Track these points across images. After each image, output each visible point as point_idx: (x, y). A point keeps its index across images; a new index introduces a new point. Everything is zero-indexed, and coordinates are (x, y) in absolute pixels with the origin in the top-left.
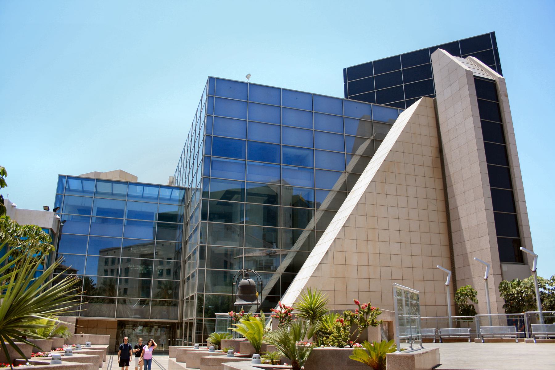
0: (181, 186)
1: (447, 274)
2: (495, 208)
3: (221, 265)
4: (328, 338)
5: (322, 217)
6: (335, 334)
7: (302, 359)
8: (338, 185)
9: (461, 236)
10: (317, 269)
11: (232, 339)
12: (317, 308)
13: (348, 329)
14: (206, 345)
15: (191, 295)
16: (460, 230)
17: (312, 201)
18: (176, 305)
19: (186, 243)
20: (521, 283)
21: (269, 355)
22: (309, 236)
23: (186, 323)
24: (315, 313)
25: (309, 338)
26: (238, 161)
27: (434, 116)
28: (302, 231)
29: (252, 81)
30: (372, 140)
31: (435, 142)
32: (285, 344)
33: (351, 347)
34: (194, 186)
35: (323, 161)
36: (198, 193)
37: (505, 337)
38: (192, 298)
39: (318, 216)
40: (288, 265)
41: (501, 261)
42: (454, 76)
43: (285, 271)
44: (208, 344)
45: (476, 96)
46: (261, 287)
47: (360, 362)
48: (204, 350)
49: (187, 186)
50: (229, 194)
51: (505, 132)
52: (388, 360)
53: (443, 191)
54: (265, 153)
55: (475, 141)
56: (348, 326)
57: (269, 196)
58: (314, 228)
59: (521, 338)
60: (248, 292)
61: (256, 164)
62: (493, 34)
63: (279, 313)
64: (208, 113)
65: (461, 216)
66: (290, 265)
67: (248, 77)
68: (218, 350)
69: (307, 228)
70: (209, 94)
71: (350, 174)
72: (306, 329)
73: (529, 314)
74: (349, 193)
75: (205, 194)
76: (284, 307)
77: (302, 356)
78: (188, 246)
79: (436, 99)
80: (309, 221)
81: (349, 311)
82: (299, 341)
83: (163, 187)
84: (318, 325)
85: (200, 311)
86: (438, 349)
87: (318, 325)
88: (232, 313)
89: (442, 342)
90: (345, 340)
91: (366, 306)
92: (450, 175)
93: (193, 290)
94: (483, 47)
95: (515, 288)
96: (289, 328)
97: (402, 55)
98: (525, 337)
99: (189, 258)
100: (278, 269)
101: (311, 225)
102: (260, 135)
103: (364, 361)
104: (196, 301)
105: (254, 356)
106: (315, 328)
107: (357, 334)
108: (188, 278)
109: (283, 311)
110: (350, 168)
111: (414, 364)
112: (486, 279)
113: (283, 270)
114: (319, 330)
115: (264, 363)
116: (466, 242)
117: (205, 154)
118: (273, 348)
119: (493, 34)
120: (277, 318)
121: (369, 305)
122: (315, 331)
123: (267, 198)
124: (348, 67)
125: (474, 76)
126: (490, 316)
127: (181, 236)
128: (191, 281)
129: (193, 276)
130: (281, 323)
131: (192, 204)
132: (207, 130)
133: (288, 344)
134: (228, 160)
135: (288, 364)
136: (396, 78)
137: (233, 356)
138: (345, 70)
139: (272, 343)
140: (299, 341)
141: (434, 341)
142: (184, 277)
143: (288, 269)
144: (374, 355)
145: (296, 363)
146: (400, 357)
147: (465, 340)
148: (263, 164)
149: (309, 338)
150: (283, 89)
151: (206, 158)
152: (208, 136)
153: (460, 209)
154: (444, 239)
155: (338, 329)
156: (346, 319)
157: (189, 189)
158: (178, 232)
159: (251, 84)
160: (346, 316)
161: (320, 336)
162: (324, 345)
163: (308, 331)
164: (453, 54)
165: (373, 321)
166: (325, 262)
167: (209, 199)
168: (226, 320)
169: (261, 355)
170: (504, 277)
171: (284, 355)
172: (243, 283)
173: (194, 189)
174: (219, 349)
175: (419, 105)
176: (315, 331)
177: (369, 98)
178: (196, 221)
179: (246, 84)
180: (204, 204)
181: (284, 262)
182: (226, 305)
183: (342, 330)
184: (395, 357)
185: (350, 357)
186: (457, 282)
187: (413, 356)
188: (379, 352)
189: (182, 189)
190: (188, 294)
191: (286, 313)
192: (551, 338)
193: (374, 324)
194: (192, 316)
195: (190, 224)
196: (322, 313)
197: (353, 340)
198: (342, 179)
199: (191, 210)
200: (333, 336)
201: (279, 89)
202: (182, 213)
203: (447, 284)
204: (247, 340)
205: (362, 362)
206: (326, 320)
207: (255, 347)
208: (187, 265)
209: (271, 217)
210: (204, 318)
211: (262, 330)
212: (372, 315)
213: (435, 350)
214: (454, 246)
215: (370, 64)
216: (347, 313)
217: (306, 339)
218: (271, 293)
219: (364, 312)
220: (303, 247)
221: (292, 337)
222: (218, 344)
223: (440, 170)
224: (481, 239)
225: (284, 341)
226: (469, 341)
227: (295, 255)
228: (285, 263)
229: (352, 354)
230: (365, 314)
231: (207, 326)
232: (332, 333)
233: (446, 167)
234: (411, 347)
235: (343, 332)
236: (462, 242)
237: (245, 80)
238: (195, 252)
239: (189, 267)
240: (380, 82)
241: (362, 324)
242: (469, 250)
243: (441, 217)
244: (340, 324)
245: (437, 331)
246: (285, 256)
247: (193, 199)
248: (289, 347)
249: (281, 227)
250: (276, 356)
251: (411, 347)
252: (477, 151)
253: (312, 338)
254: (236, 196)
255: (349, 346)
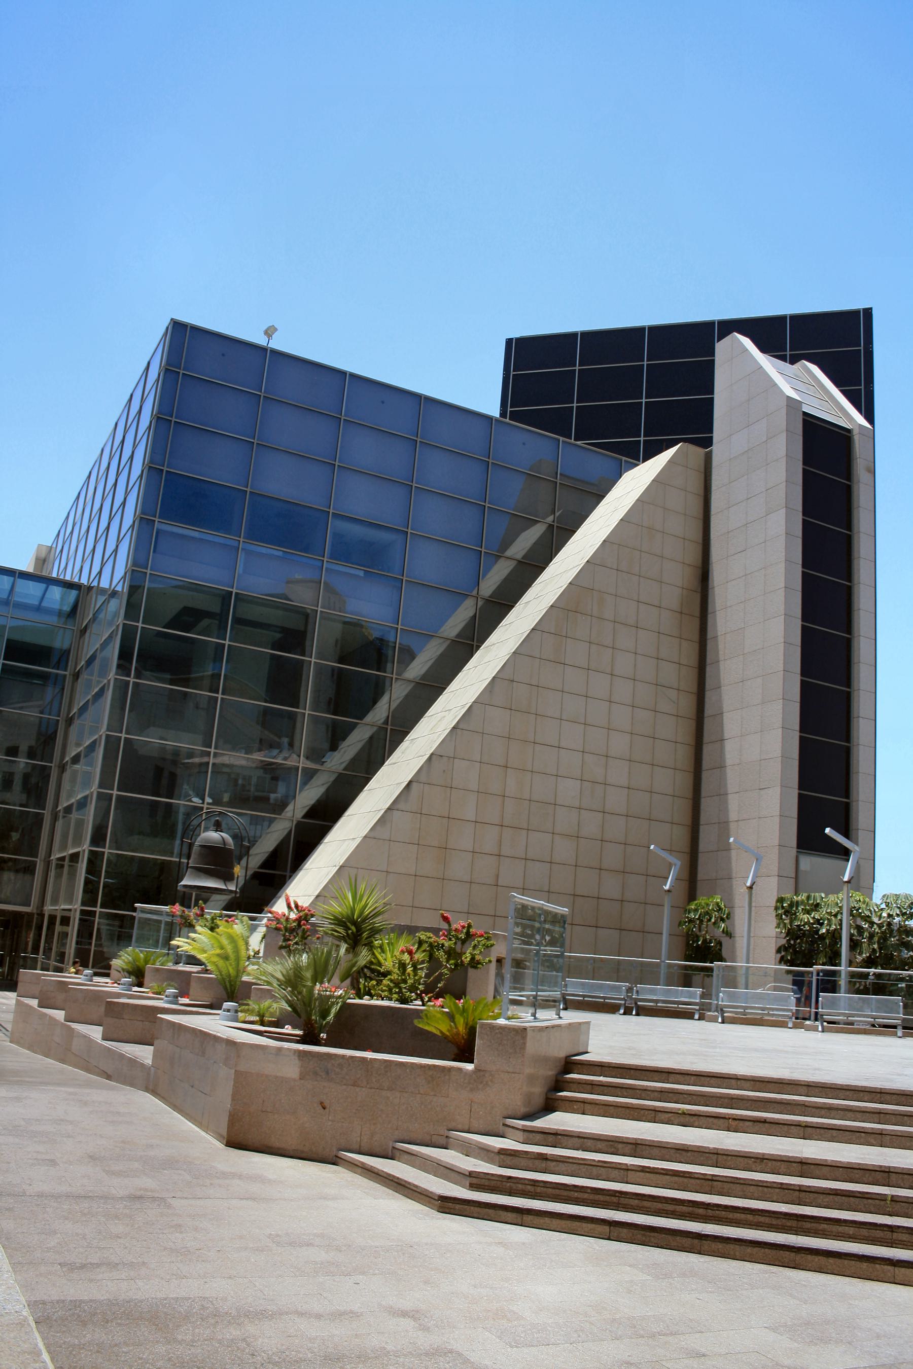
0: (68, 578)
1: (670, 865)
2: (803, 728)
3: (149, 782)
4: (379, 982)
5: (407, 696)
6: (394, 977)
7: (324, 1019)
8: (454, 626)
9: (722, 780)
10: (381, 821)
11: (170, 966)
12: (364, 920)
13: (422, 969)
14: (107, 975)
15: (71, 851)
16: (721, 766)
17: (392, 639)
18: (29, 869)
19: (70, 721)
20: (834, 905)
21: (256, 1007)
22: (371, 738)
23: (52, 918)
24: (359, 930)
25: (342, 981)
26: (221, 541)
27: (702, 492)
28: (353, 727)
29: (278, 343)
30: (551, 527)
31: (693, 555)
32: (294, 987)
33: (423, 1005)
34: (104, 584)
35: (427, 563)
36: (113, 604)
37: (768, 1014)
38: (75, 857)
39: (397, 693)
40: (312, 802)
41: (798, 847)
42: (764, 392)
43: (305, 816)
44: (113, 972)
45: (801, 463)
46: (244, 851)
47: (435, 1035)
48: (104, 985)
49: (84, 581)
50: (188, 617)
51: (855, 554)
52: (480, 1033)
53: (696, 671)
54: (289, 528)
55: (782, 566)
56: (423, 962)
57: (284, 630)
58: (386, 722)
59: (800, 1020)
60: (218, 861)
61: (264, 550)
62: (868, 313)
63: (283, 920)
64: (159, 412)
65: (726, 735)
66: (319, 802)
67: (270, 332)
68: (136, 989)
69: (369, 718)
70: (168, 363)
71: (488, 601)
72: (337, 963)
73: (822, 971)
74: (478, 647)
75: (131, 609)
76: (297, 906)
77: (324, 1014)
78: (74, 730)
79: (711, 451)
80: (375, 702)
81: (429, 934)
82: (322, 983)
83: (24, 575)
84: (364, 956)
85: (90, 889)
86: (588, 1023)
87: (364, 956)
88: (177, 909)
89: (637, 1014)
90: (413, 989)
91: (463, 927)
92: (716, 637)
93: (78, 841)
94: (838, 343)
95: (808, 912)
96: (305, 956)
97: (652, 329)
98: (809, 1019)
99: (76, 759)
100: (290, 808)
101: (380, 712)
102: (282, 481)
103: (441, 1032)
104: (83, 866)
105: (226, 1005)
106: (356, 962)
107: (438, 979)
108: (68, 810)
109: (293, 916)
110: (489, 585)
111: (525, 1044)
112: (751, 888)
113: (299, 814)
114: (365, 966)
115: (245, 1022)
116: (730, 797)
117: (143, 513)
118: (269, 994)
119: (868, 313)
120: (277, 929)
121: (469, 926)
122: (355, 969)
123: (278, 636)
124: (518, 336)
125: (805, 414)
126: (748, 968)
127: (56, 704)
128: (74, 816)
129: (83, 804)
130: (286, 940)
131: (95, 628)
132: (153, 451)
133: (300, 988)
134: (196, 535)
135: (294, 1027)
136: (628, 382)
137: (177, 1004)
138: (509, 342)
139: (269, 983)
140: (322, 983)
141: (622, 1011)
142: (56, 805)
143: (312, 813)
144: (460, 1021)
145: (312, 1025)
146: (502, 1028)
147: (688, 1015)
148: (280, 554)
149: (342, 981)
150: (353, 376)
151: (144, 521)
152: (152, 469)
153: (727, 717)
154: (684, 781)
155: (403, 966)
156: (422, 949)
157: (90, 588)
158: (50, 692)
159: (275, 352)
160: (421, 943)
161: (365, 977)
162: (372, 996)
163: (343, 966)
164: (763, 350)
165: (473, 959)
166: (401, 806)
167: (140, 625)
168: (160, 922)
169: (240, 1005)
170: (801, 885)
171: (289, 1009)
172: (207, 840)
173: (103, 591)
174: (140, 985)
175: (657, 481)
176: (355, 969)
177: (555, 424)
178: (103, 672)
179: (264, 349)
180: (128, 635)
181: (305, 794)
182: (160, 885)
183: (410, 969)
184: (492, 1027)
185: (416, 1022)
186: (699, 884)
187: (525, 1029)
188: (470, 1019)
189: (69, 585)
190: (64, 847)
191: (299, 920)
192: (880, 1026)
193: (474, 963)
194: (71, 903)
195: (84, 676)
196: (375, 932)
197: (432, 990)
198: (465, 612)
199: (91, 644)
200: (391, 981)
201: (343, 373)
202: (66, 646)
203: (667, 887)
204: (206, 971)
205: (438, 1033)
206: (381, 947)
207: (225, 988)
208: (67, 776)
209: (284, 683)
210: (98, 909)
211: (243, 953)
212: (475, 947)
213: (580, 1024)
214: (703, 800)
215: (570, 338)
216: (423, 937)
217: (336, 980)
218: (265, 865)
219: (457, 938)
220: (353, 763)
221: (308, 974)
222: (138, 975)
223: (697, 622)
224: (762, 792)
225: (293, 981)
226: (697, 1017)
227: (332, 779)
228: (308, 796)
229: (420, 1018)
230: (459, 943)
231: (104, 928)
232: (388, 973)
233: (710, 617)
234: (534, 1015)
235: (412, 973)
236: (722, 795)
237: (261, 341)
238: (92, 747)
239: (73, 780)
240: (592, 385)
241: (452, 962)
242: (733, 816)
243: (684, 732)
244: (406, 957)
245: (630, 990)
246: (310, 775)
247: (102, 616)
248: (300, 993)
249: (306, 711)
250: (271, 1010)
251: (534, 1015)
252: (782, 593)
253: (348, 981)
254: (205, 622)
255: (420, 1003)
